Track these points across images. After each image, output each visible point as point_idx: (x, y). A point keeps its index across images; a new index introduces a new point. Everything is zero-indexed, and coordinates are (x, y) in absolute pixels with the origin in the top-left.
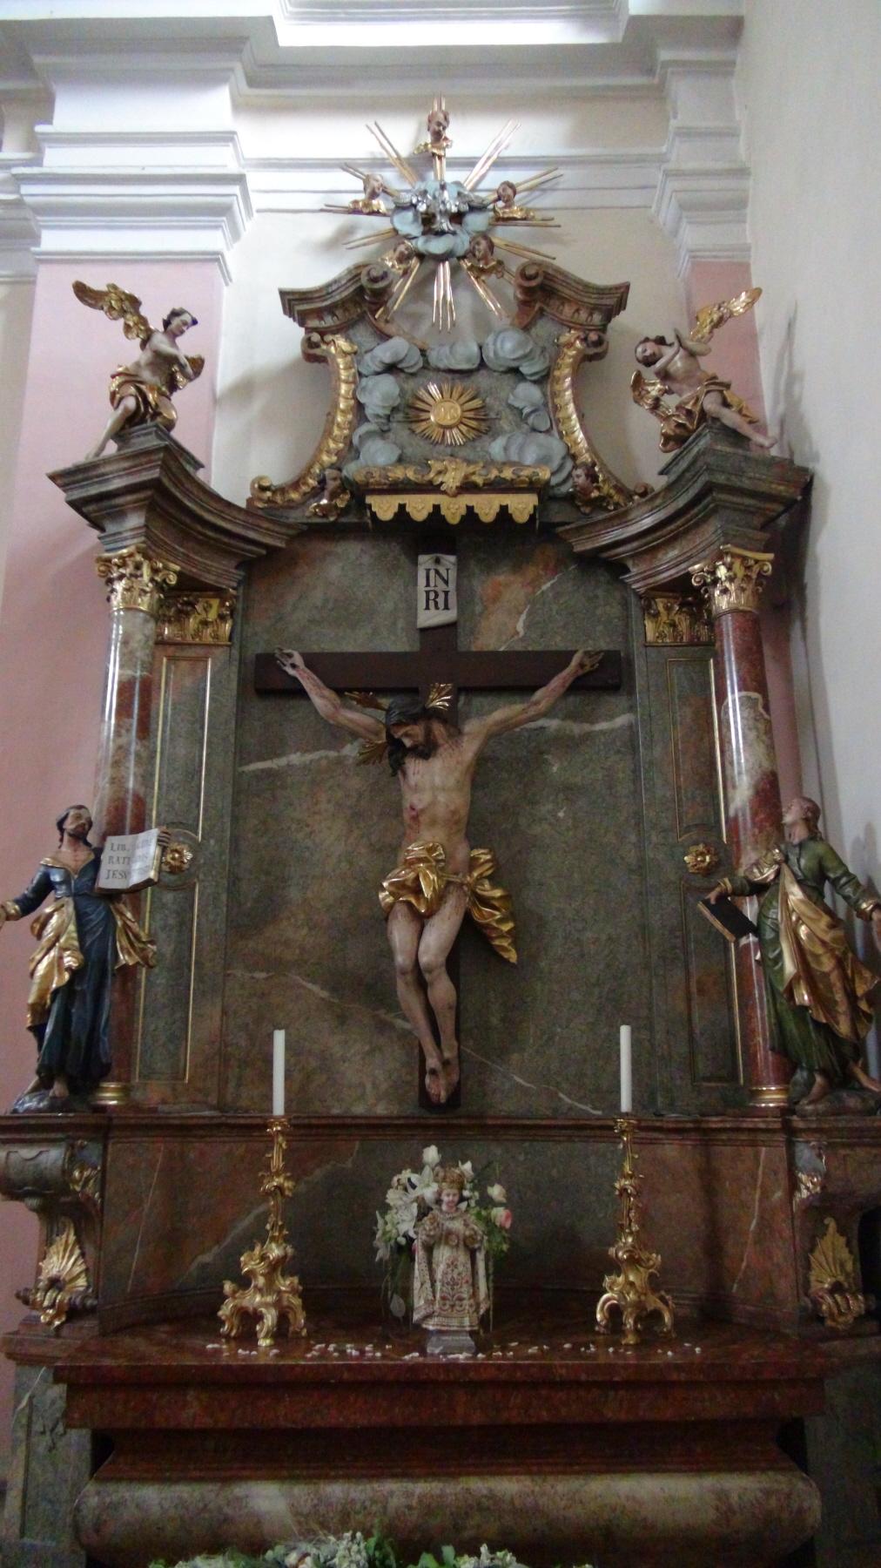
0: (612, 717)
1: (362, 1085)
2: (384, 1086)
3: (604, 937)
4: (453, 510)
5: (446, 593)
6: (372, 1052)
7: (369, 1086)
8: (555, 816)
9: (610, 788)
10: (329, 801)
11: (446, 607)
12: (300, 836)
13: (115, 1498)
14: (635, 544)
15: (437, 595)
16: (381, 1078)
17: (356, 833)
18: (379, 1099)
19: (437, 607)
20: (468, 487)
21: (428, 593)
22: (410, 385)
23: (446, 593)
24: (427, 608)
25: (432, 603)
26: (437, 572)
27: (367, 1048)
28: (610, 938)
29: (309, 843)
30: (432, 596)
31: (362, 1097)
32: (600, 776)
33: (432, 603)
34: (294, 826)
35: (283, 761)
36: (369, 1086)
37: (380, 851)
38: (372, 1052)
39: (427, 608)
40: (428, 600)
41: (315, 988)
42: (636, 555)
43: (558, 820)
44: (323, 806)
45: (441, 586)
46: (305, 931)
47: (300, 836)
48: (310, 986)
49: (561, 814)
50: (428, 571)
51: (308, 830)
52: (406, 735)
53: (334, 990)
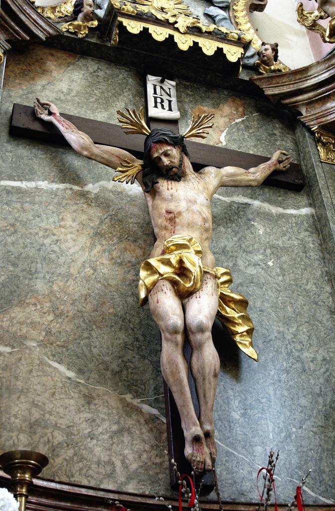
0: (298, 208)
1: (110, 463)
2: (134, 466)
3: (320, 358)
4: (184, 43)
5: (170, 102)
6: (120, 432)
7: (118, 464)
8: (266, 264)
9: (305, 252)
10: (74, 221)
11: (170, 109)
12: (47, 241)
13: (120, 473)
14: (311, 94)
15: (162, 101)
16: (131, 457)
17: (99, 247)
18: (129, 478)
19: (163, 107)
20: (195, 30)
21: (155, 98)
22: (27, 96)
23: (170, 102)
24: (156, 106)
25: (159, 105)
26: (161, 88)
27: (115, 428)
28: (324, 360)
29: (56, 248)
30: (159, 100)
31: (111, 475)
32: (296, 243)
33: (159, 105)
34: (41, 234)
35: (31, 185)
36: (118, 464)
37: (120, 264)
38: (120, 432)
39: (156, 106)
40: (156, 102)
41: (62, 368)
42: (310, 103)
43: (269, 267)
44: (69, 223)
45: (165, 97)
46: (51, 317)
47: (47, 241)
48: (56, 365)
49: (270, 263)
50: (155, 86)
51: (55, 238)
52: (166, 154)
53: (80, 372)
